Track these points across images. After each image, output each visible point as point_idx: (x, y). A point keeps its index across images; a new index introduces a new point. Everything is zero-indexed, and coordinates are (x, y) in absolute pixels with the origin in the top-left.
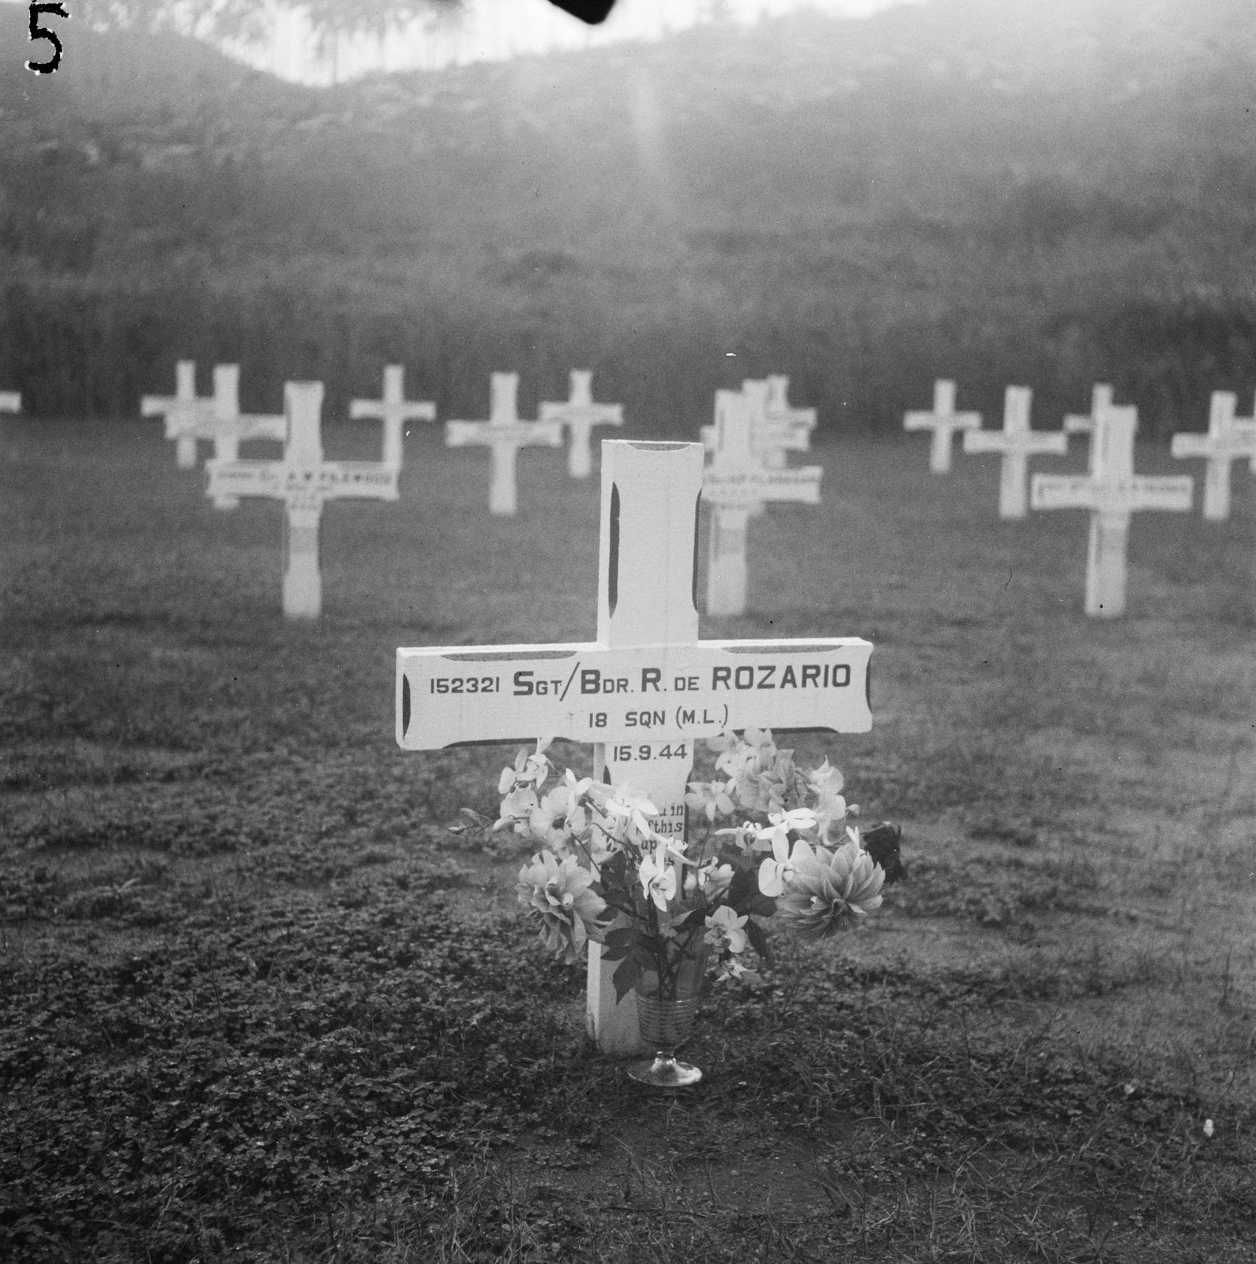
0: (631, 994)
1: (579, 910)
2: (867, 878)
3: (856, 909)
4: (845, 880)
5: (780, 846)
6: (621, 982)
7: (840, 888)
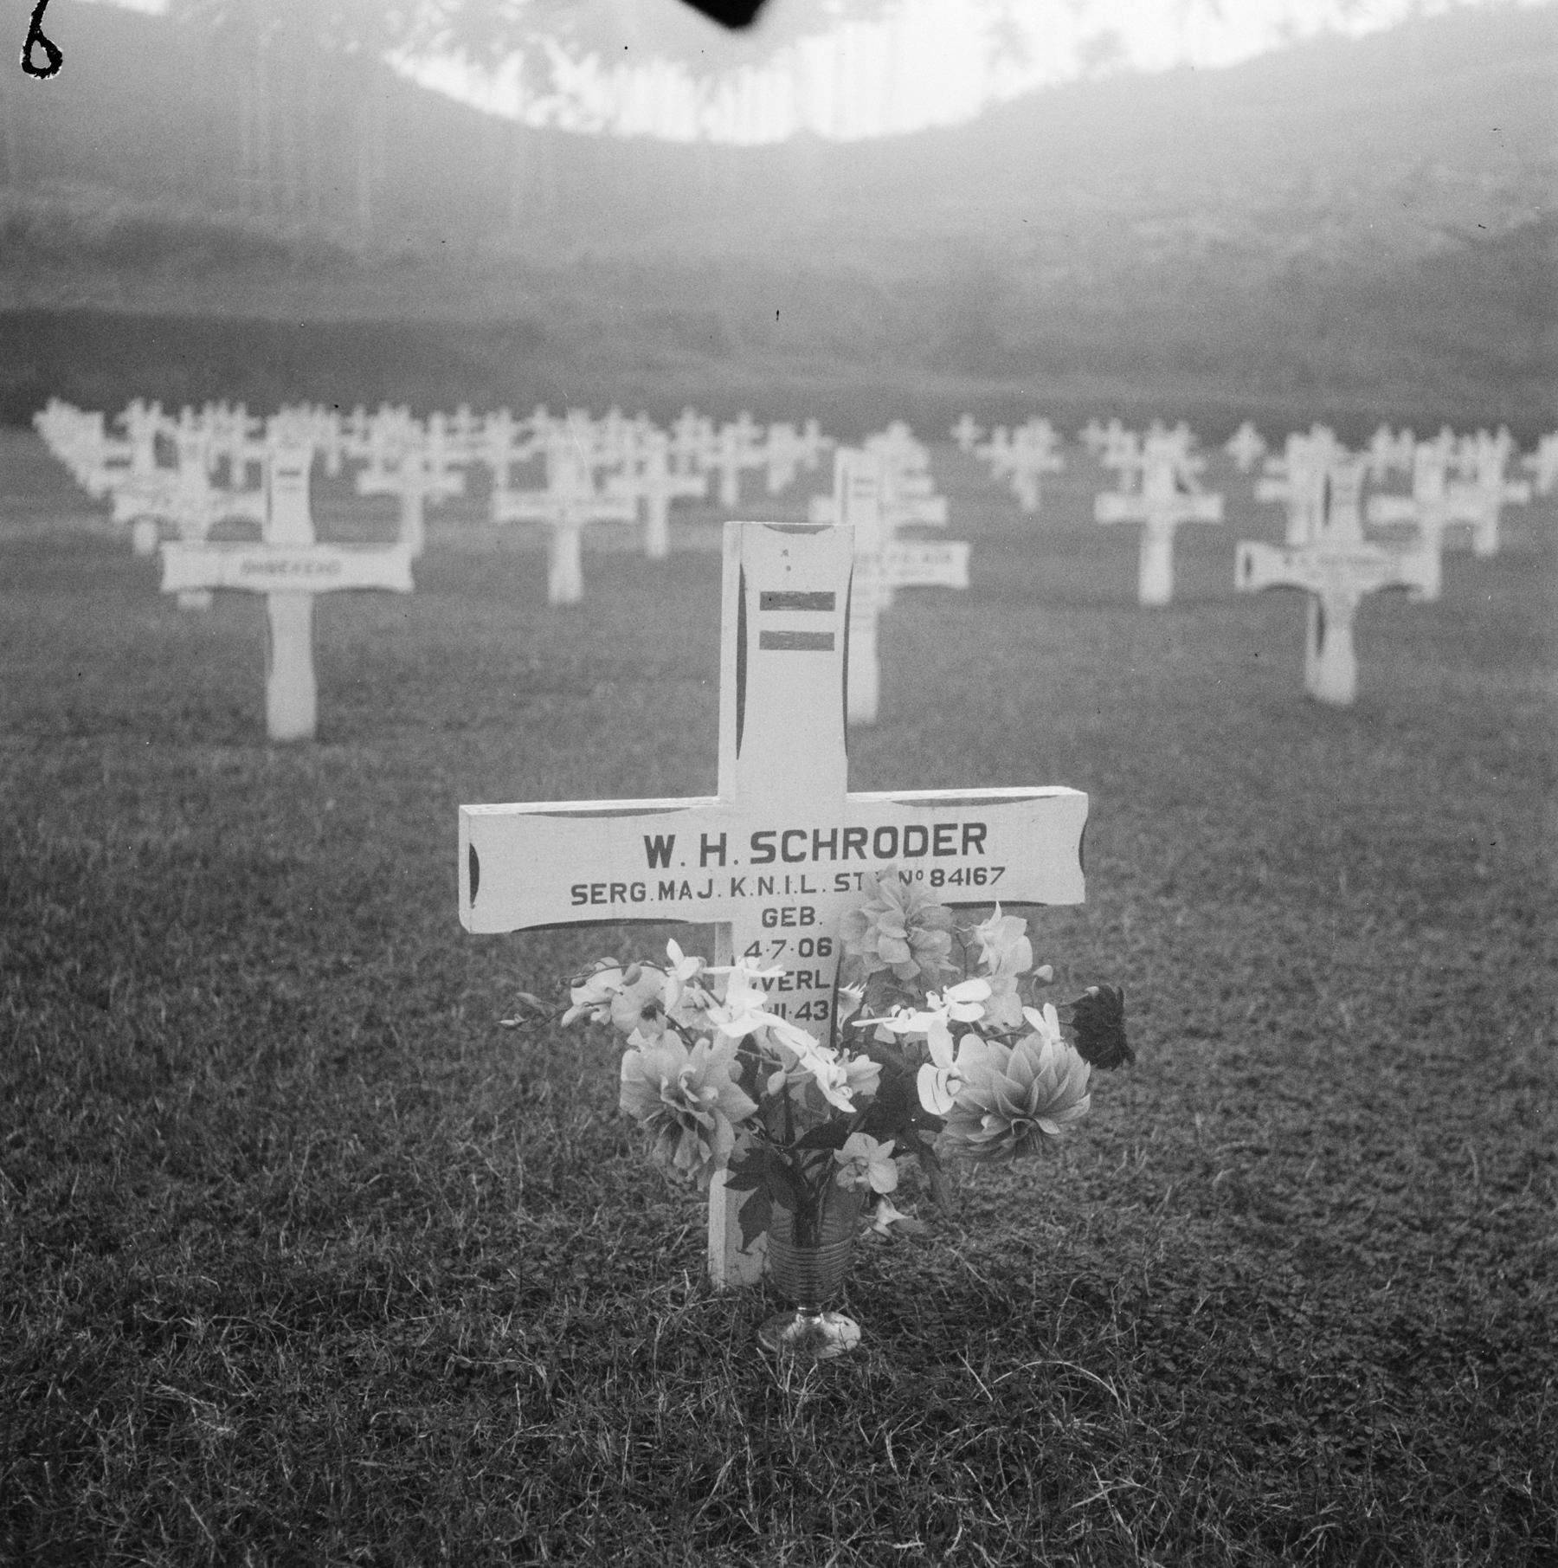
0: (762, 1240)
1: (723, 1109)
2: (1060, 1082)
3: (1048, 1127)
4: (1028, 1087)
5: (940, 1045)
6: (750, 1221)
7: (1022, 1101)
